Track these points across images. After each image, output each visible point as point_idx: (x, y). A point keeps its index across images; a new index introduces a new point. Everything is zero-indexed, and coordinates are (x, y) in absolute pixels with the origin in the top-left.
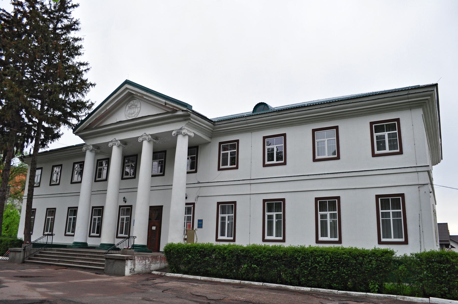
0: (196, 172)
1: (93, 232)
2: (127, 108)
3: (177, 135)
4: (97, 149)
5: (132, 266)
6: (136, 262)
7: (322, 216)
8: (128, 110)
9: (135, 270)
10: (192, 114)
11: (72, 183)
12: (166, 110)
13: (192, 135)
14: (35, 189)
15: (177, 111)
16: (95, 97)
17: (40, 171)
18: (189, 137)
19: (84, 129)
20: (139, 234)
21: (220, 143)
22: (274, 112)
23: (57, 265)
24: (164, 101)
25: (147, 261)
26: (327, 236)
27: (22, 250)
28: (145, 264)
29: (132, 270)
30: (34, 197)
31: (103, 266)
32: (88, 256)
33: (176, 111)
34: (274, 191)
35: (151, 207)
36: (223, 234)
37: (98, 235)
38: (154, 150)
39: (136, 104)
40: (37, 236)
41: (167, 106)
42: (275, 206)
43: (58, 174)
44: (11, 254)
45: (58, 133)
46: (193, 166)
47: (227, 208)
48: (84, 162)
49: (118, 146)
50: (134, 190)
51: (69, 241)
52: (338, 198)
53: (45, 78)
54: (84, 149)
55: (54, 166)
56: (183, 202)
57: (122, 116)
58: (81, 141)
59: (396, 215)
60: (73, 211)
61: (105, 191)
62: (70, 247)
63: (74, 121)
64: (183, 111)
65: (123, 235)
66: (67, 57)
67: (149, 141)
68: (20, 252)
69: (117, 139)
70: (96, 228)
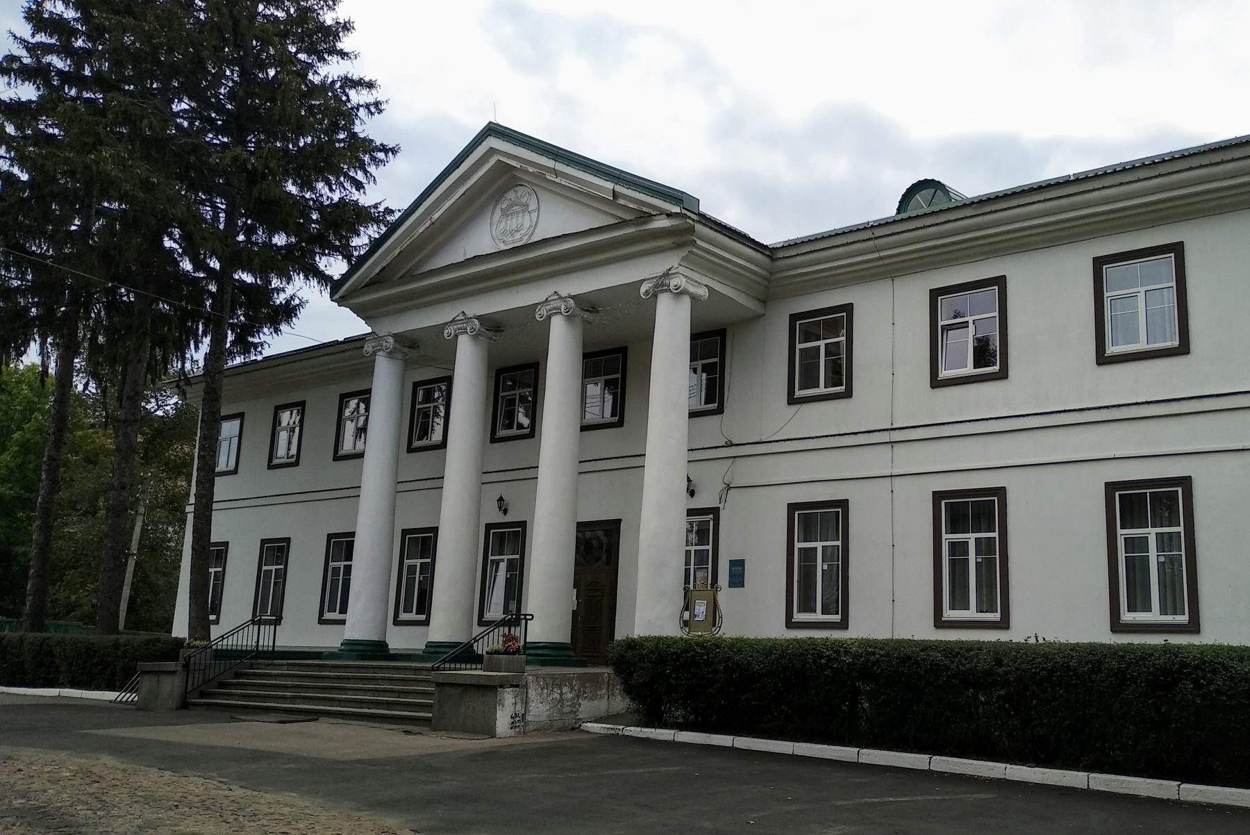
0: (720, 410)
1: (408, 610)
2: (498, 213)
3: (655, 296)
4: (410, 347)
5: (519, 707)
6: (532, 693)
7: (1131, 543)
8: (500, 222)
9: (529, 718)
10: (698, 227)
11: (337, 458)
12: (617, 217)
13: (702, 292)
14: (218, 481)
15: (653, 217)
16: (391, 188)
17: (237, 423)
18: (694, 299)
19: (367, 285)
20: (548, 611)
21: (794, 318)
22: (965, 205)
23: (286, 710)
24: (610, 185)
25: (565, 689)
26: (1147, 608)
27: (179, 668)
28: (561, 700)
29: (519, 721)
30: (215, 506)
31: (427, 707)
32: (383, 679)
33: (649, 217)
34: (968, 464)
35: (581, 526)
36: (960, 601)
37: (423, 617)
38: (585, 346)
39: (524, 200)
40: (234, 621)
41: (621, 202)
42: (971, 514)
43: (293, 430)
44: (147, 683)
45: (288, 302)
46: (713, 395)
47: (820, 520)
48: (369, 391)
49: (475, 337)
50: (529, 472)
51: (330, 639)
52: (1186, 482)
53: (237, 125)
54: (368, 347)
55: (279, 409)
56: (676, 507)
57: (483, 239)
58: (359, 327)
59: (1165, 542)
60: (341, 546)
61: (436, 481)
62: (332, 656)
63: (335, 266)
64: (670, 215)
65: (412, 616)
66: (302, 56)
67: (570, 318)
68: (174, 672)
69: (470, 313)
70: (416, 597)
